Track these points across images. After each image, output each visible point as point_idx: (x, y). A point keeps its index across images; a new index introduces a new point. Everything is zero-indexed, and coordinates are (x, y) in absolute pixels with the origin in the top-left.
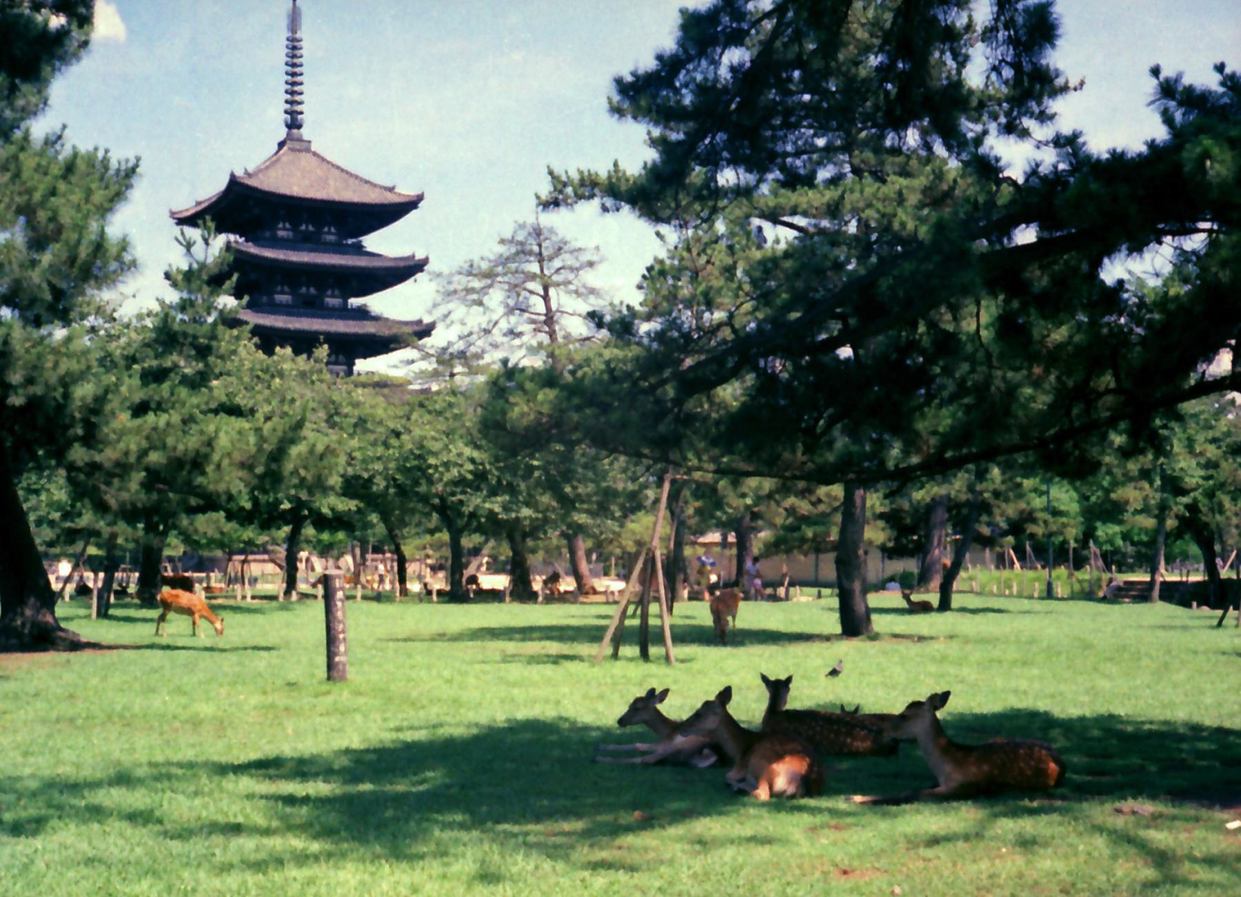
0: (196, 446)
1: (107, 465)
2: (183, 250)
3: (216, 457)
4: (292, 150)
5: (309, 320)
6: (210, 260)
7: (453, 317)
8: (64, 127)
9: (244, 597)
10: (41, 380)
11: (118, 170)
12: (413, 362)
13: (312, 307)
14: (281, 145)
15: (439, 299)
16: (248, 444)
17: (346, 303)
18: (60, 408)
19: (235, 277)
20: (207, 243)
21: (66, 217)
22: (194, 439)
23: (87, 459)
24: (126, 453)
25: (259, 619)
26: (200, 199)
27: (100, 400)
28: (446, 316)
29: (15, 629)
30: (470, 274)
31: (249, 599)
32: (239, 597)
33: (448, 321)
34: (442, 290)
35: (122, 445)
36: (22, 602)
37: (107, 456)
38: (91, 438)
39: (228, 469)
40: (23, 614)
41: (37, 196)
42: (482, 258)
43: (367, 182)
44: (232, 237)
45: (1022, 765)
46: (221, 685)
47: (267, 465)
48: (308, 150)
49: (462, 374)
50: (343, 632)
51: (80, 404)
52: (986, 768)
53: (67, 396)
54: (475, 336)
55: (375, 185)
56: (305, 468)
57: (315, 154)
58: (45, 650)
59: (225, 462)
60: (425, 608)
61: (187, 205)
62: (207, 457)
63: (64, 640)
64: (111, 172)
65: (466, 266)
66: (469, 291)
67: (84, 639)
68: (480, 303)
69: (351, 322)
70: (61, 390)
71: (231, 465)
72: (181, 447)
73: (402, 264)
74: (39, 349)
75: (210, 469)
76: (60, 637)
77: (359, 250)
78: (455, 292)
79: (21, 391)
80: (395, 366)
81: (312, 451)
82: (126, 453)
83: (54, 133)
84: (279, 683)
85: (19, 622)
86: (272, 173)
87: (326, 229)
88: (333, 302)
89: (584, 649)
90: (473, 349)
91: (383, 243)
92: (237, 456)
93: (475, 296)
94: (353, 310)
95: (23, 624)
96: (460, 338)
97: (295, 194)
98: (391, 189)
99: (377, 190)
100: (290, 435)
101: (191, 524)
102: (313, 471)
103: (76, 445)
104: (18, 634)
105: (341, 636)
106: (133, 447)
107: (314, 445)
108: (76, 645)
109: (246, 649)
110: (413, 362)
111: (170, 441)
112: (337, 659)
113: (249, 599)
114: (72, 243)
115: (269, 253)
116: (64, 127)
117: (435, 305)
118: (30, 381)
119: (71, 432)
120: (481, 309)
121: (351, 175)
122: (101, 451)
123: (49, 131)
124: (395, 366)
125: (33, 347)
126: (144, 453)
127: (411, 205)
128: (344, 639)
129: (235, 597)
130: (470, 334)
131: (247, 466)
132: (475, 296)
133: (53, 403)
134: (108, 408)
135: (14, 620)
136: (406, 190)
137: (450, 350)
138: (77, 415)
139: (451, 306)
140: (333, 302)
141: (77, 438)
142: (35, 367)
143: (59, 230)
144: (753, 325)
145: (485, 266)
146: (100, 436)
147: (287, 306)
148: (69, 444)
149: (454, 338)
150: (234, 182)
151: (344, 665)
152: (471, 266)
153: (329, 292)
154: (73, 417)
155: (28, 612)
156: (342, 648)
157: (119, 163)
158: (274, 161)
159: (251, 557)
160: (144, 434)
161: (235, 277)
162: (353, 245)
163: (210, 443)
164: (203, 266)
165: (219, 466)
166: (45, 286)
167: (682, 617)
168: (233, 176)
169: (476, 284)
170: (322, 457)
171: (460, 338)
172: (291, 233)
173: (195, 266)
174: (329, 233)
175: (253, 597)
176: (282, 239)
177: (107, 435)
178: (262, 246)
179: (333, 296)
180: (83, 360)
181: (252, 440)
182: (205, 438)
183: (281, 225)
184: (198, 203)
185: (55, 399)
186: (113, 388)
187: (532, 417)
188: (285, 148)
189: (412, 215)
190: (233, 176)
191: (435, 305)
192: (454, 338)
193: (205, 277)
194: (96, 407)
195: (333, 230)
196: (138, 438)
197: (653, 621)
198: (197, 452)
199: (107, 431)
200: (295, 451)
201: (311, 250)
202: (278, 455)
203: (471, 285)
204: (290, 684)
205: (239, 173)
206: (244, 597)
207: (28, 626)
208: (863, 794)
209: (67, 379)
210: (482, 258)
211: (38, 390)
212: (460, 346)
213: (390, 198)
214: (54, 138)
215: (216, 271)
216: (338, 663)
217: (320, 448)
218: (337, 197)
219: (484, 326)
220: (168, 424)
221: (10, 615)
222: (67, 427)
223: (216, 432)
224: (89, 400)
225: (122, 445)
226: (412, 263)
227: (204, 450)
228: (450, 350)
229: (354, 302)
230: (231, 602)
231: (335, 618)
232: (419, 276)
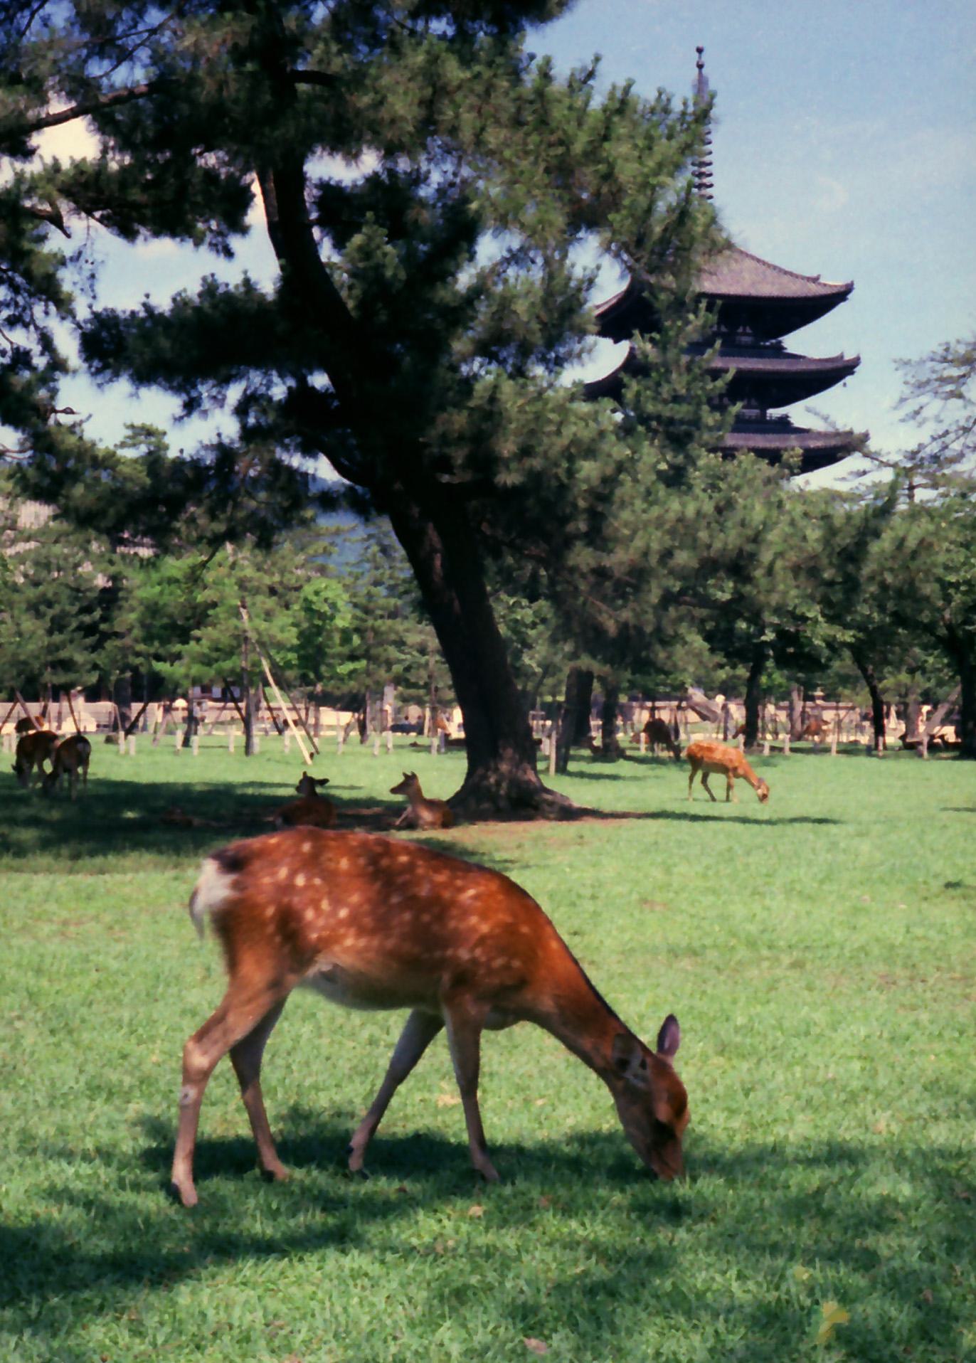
0: (738, 542)
1: (618, 573)
3: (766, 557)
7: (924, 413)
8: (597, 59)
10: (540, 449)
11: (684, 114)
12: (865, 473)
15: (907, 391)
17: (764, 414)
18: (563, 488)
21: (627, 172)
23: (593, 564)
24: (646, 554)
27: (610, 481)
28: (917, 413)
29: (488, 789)
30: (944, 360)
33: (919, 418)
34: (913, 381)
35: (639, 543)
36: (496, 755)
37: (619, 559)
38: (597, 537)
40: (497, 770)
41: (578, 148)
42: (958, 342)
43: (786, 273)
49: (924, 486)
51: (585, 487)
53: (571, 473)
54: (952, 436)
55: (797, 276)
58: (529, 818)
59: (779, 564)
60: (908, 766)
62: (752, 556)
63: (551, 804)
64: (673, 116)
65: (940, 351)
66: (943, 380)
67: (576, 804)
68: (960, 396)
69: (770, 436)
70: (565, 465)
72: (718, 545)
73: (829, 366)
74: (539, 405)
75: (758, 573)
76: (546, 801)
77: (779, 351)
78: (928, 382)
79: (514, 465)
80: (844, 479)
82: (646, 554)
83: (584, 69)
84: (936, 885)
85: (492, 780)
87: (740, 330)
90: (948, 453)
91: (808, 343)
93: (949, 388)
95: (498, 784)
96: (934, 439)
98: (815, 280)
99: (799, 282)
101: (669, 657)
103: (579, 545)
104: (492, 797)
106: (655, 546)
108: (569, 813)
110: (865, 473)
111: (703, 535)
114: (639, 212)
116: (597, 59)
117: (903, 400)
118: (526, 452)
119: (570, 528)
120: (959, 402)
121: (769, 266)
122: (611, 551)
123: (578, 65)
124: (844, 479)
125: (529, 402)
126: (667, 554)
127: (839, 296)
130: (947, 433)
131: (808, 570)
132: (949, 388)
133: (554, 483)
134: (618, 492)
135: (485, 777)
136: (833, 280)
137: (921, 454)
138: (582, 504)
139: (924, 399)
141: (577, 536)
142: (532, 433)
143: (619, 192)
145: (962, 350)
146: (607, 531)
148: (568, 542)
149: (926, 440)
152: (947, 350)
154: (575, 506)
155: (504, 767)
157: (685, 104)
159: (658, 704)
160: (667, 526)
162: (772, 346)
165: (770, 571)
166: (535, 326)
169: (955, 372)
170: (914, 555)
171: (934, 439)
174: (745, 334)
177: (617, 530)
180: (592, 424)
185: (557, 477)
186: (627, 465)
189: (841, 308)
191: (903, 400)
192: (926, 440)
193: (684, 344)
194: (603, 494)
195: (748, 330)
196: (659, 534)
198: (741, 550)
199: (621, 520)
203: (946, 374)
204: (949, 885)
207: (504, 785)
209: (573, 450)
210: (958, 342)
211: (536, 463)
212: (934, 448)
213: (814, 290)
214: (583, 76)
217: (911, 543)
218: (754, 292)
219: (962, 423)
220: (698, 513)
221: (480, 771)
222: (565, 520)
224: (595, 482)
225: (639, 543)
226: (839, 364)
227: (749, 547)
228: (921, 454)
229: (774, 413)
232: (848, 379)
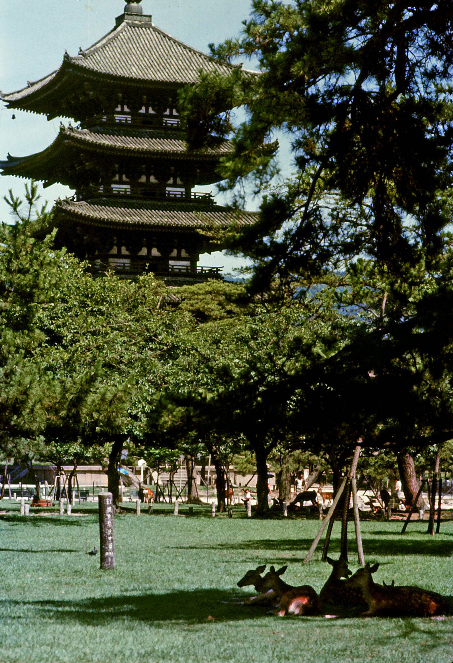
2: (12, 209)
4: (133, 26)
5: (148, 212)
6: (34, 218)
9: (66, 511)
13: (152, 197)
14: (119, 20)
16: (55, 393)
17: (188, 192)
19: (55, 231)
20: (31, 203)
22: (14, 389)
25: (75, 530)
26: (32, 80)
31: (69, 513)
32: (62, 511)
39: (40, 412)
44: (68, 122)
45: (413, 601)
46: (28, 571)
47: (69, 410)
48: (148, 26)
50: (111, 535)
52: (391, 602)
56: (98, 411)
57: (155, 30)
61: (18, 86)
62: (24, 402)
69: (193, 214)
71: (41, 409)
75: (26, 412)
81: (103, 399)
86: (108, 52)
87: (168, 113)
88: (175, 191)
89: (300, 554)
92: (46, 402)
94: (196, 200)
97: (134, 75)
100: (86, 387)
102: (104, 414)
105: (110, 538)
107: (104, 394)
109: (53, 551)
112: (107, 554)
113: (69, 513)
115: (105, 141)
128: (112, 540)
129: (59, 510)
140: (175, 191)
144: (293, 372)
147: (125, 196)
150: (68, 62)
151: (112, 558)
153: (171, 181)
156: (110, 547)
158: (111, 39)
161: (55, 231)
163: (25, 393)
164: (27, 223)
165: (32, 411)
167: (370, 533)
168: (67, 57)
170: (111, 402)
172: (129, 117)
173: (21, 222)
175: (73, 511)
176: (120, 124)
178: (98, 132)
179: (175, 185)
181: (58, 389)
182: (21, 389)
183: (119, 109)
184: (32, 84)
187: (170, 423)
188: (124, 24)
190: (67, 57)
197: (350, 537)
200: (90, 398)
201: (152, 136)
202: (78, 401)
205: (74, 54)
206: (66, 511)
208: (331, 614)
215: (37, 227)
216: (107, 557)
223: (31, 383)
229: (199, 190)
230: (55, 515)
231: (106, 526)
